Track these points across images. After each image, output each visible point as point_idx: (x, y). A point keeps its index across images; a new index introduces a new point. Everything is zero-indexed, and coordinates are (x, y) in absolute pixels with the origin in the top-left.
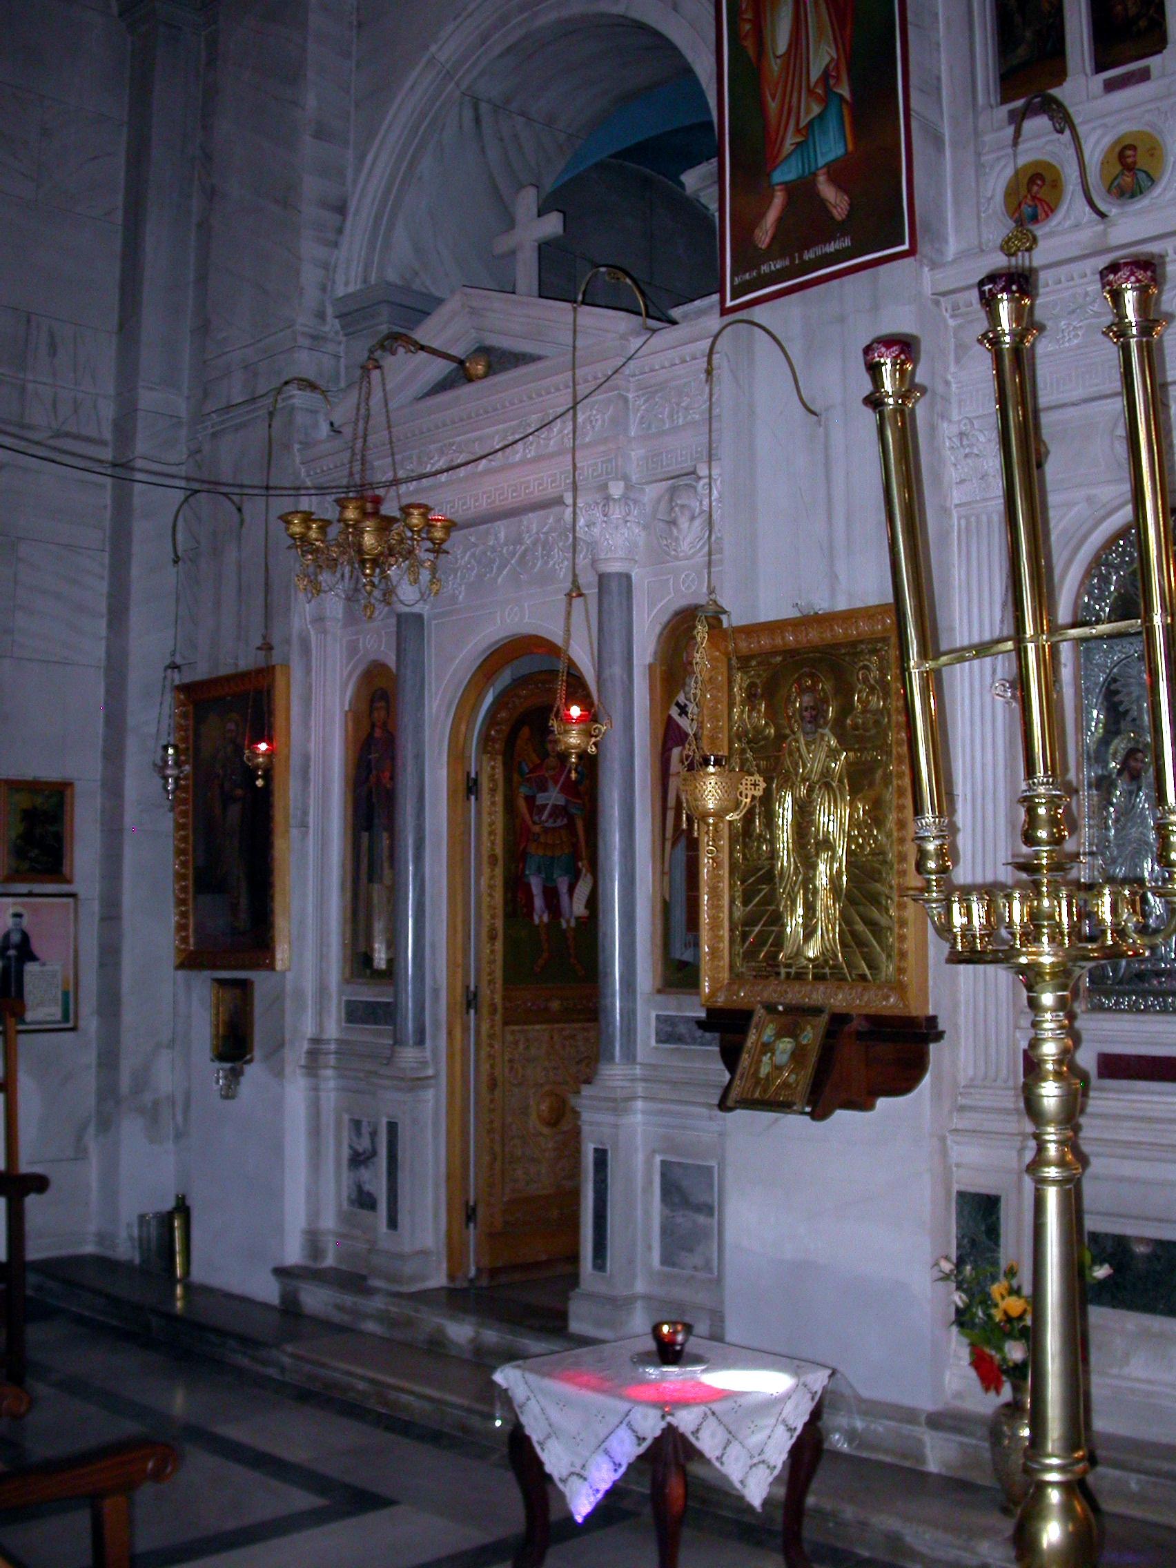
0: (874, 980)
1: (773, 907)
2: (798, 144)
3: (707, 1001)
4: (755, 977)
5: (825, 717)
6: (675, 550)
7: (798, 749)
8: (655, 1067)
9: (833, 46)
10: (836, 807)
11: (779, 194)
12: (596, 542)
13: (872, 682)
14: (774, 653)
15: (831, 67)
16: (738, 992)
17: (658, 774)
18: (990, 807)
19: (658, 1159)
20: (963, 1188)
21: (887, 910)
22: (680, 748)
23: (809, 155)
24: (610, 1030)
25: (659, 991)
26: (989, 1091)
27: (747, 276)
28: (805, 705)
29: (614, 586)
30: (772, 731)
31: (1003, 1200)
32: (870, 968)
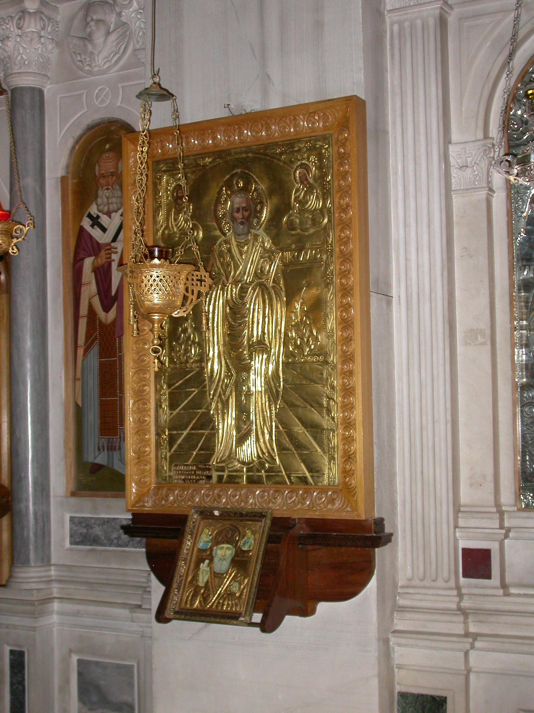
0: (316, 484)
1: (204, 410)
3: (134, 506)
4: (184, 480)
5: (259, 218)
6: (89, 65)
7: (229, 250)
8: (69, 567)
10: (271, 305)
12: (9, 57)
13: (311, 181)
14: (203, 155)
16: (167, 496)
17: (70, 285)
18: (426, 307)
19: (75, 658)
20: (404, 689)
21: (329, 411)
22: (92, 258)
24: (26, 534)
25: (73, 494)
26: (431, 592)
28: (236, 206)
29: (27, 100)
30: (201, 235)
31: (448, 700)
32: (310, 471)
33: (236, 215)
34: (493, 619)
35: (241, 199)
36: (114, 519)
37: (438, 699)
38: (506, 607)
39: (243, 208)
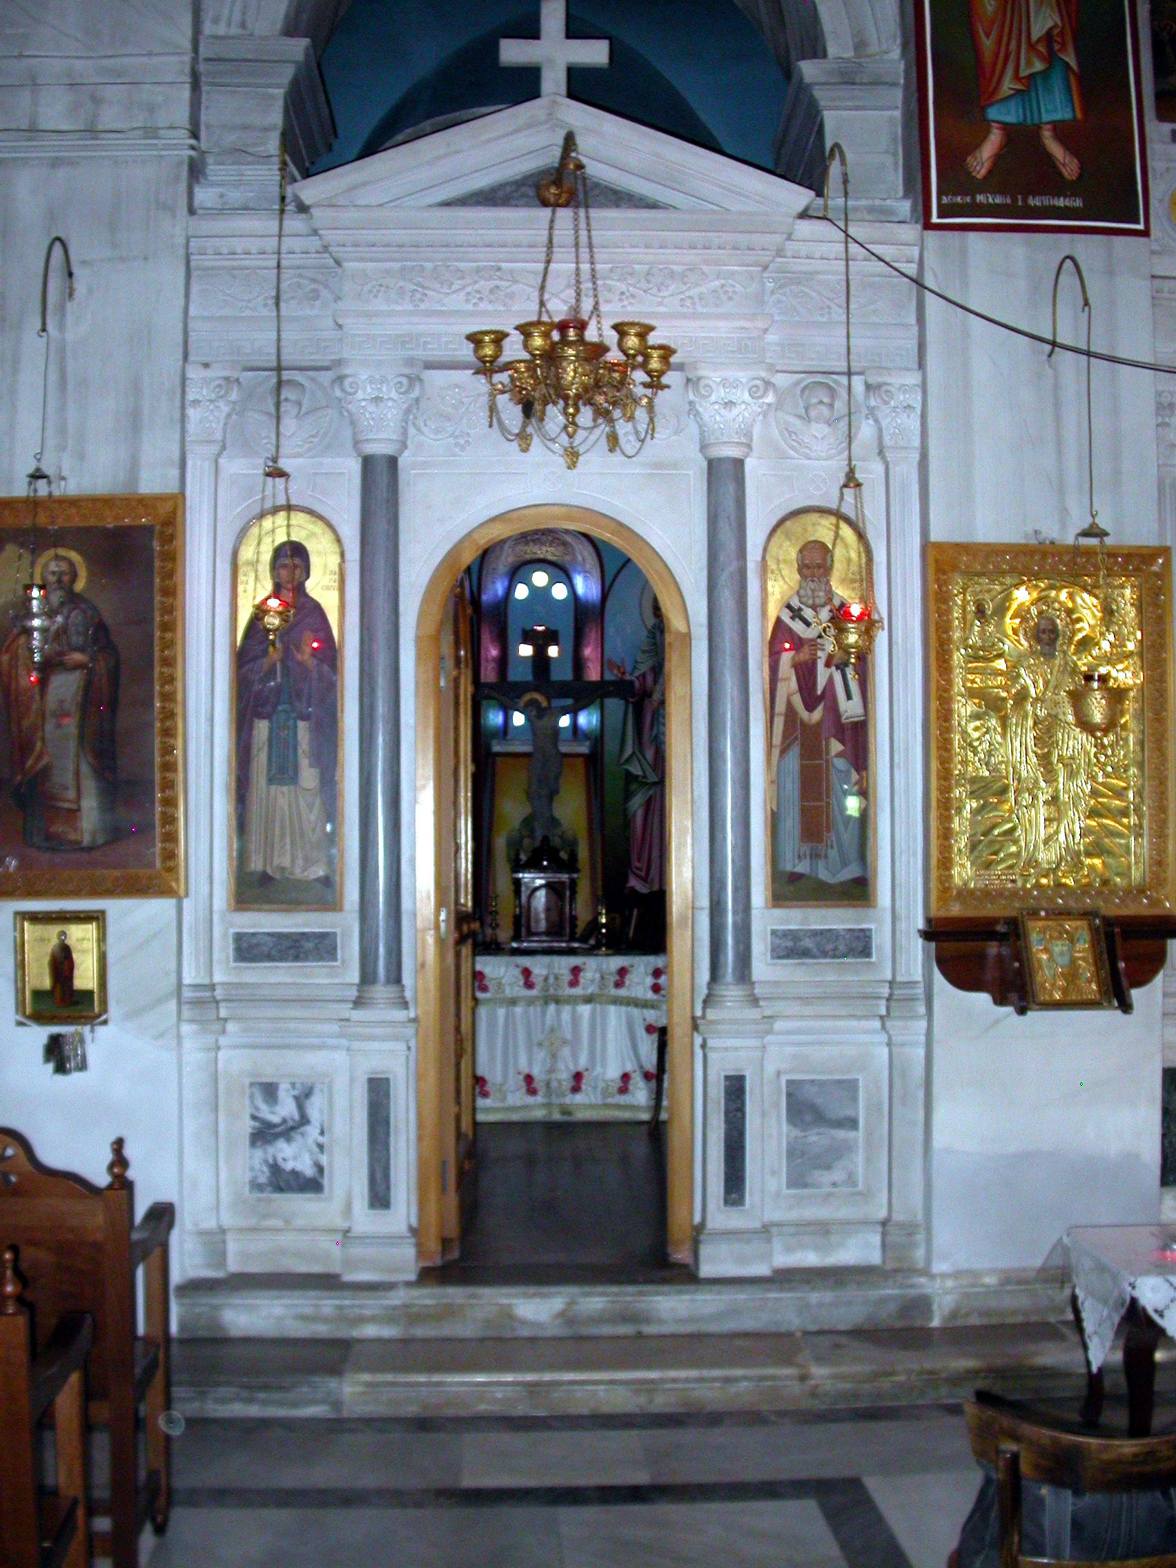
2: (1018, 91)
9: (1056, 9)
11: (995, 131)
15: (1056, 31)
23: (1031, 105)
27: (959, 199)
36: (830, 930)
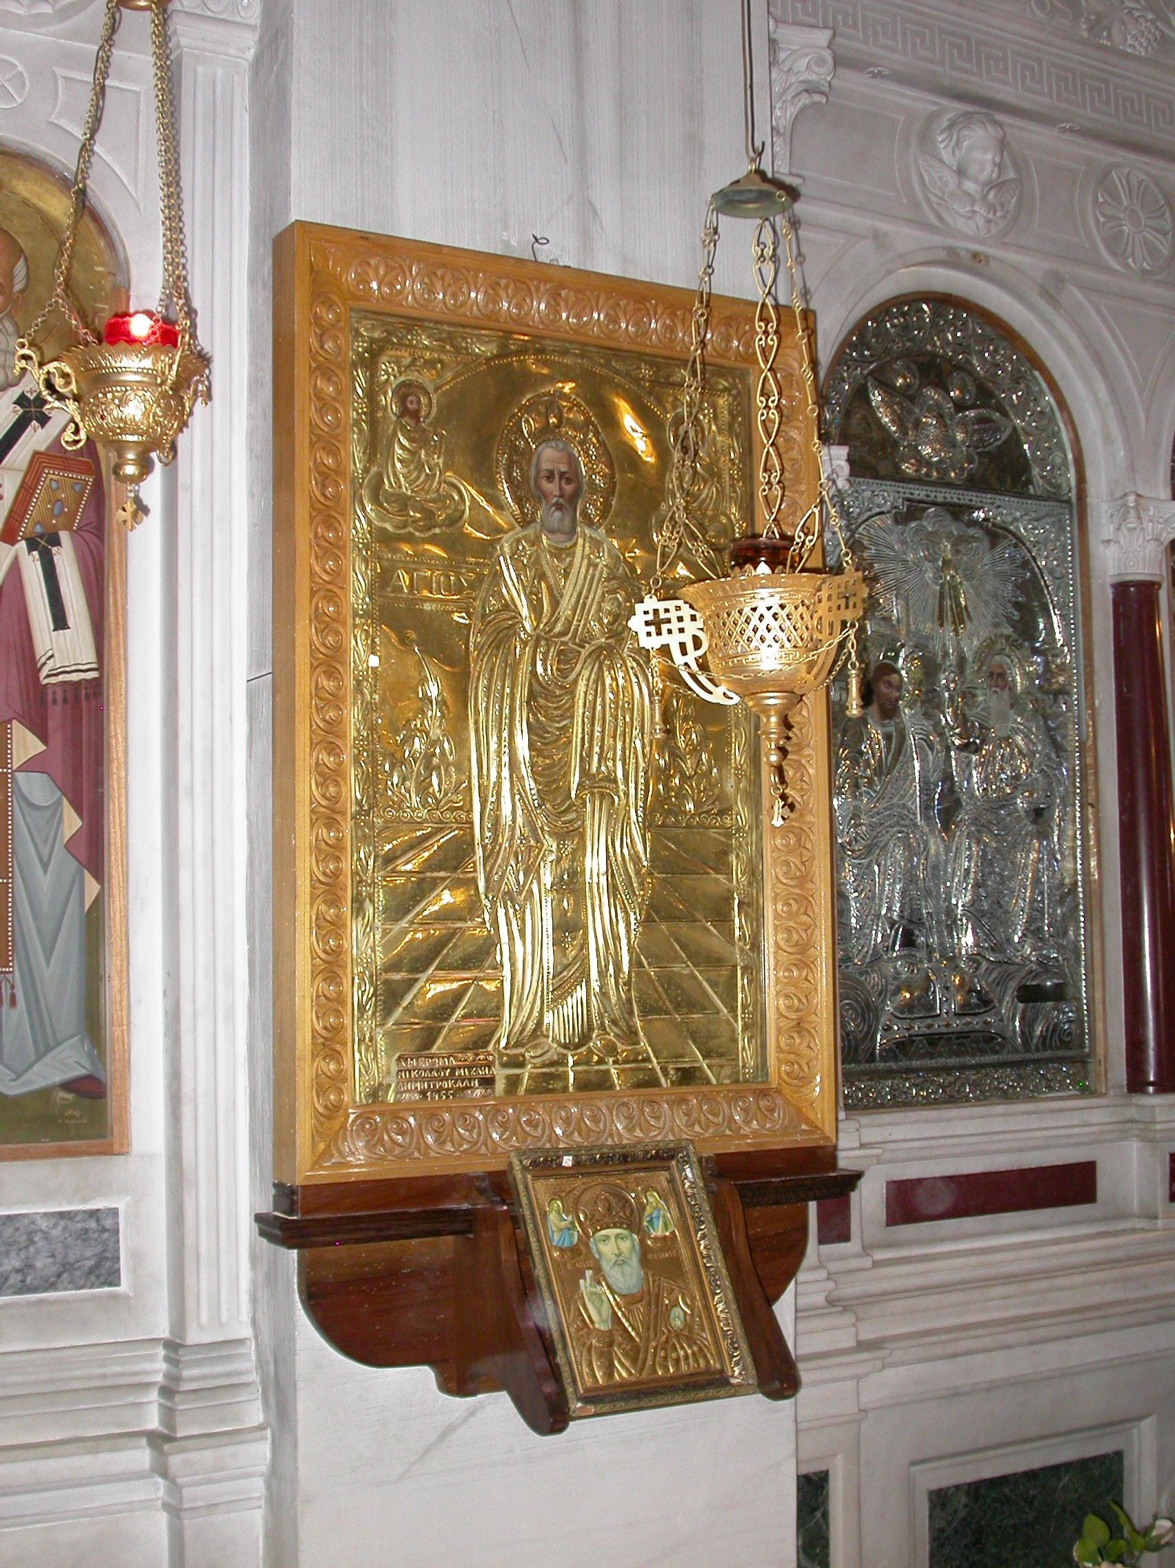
4: (423, 1093)
33: (547, 486)
34: (876, 1310)
35: (557, 454)
37: (815, 1478)
38: (887, 1286)
39: (562, 474)
